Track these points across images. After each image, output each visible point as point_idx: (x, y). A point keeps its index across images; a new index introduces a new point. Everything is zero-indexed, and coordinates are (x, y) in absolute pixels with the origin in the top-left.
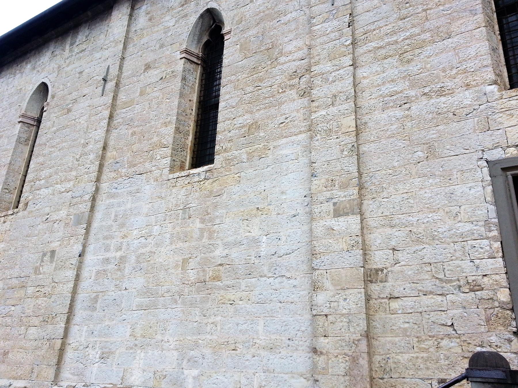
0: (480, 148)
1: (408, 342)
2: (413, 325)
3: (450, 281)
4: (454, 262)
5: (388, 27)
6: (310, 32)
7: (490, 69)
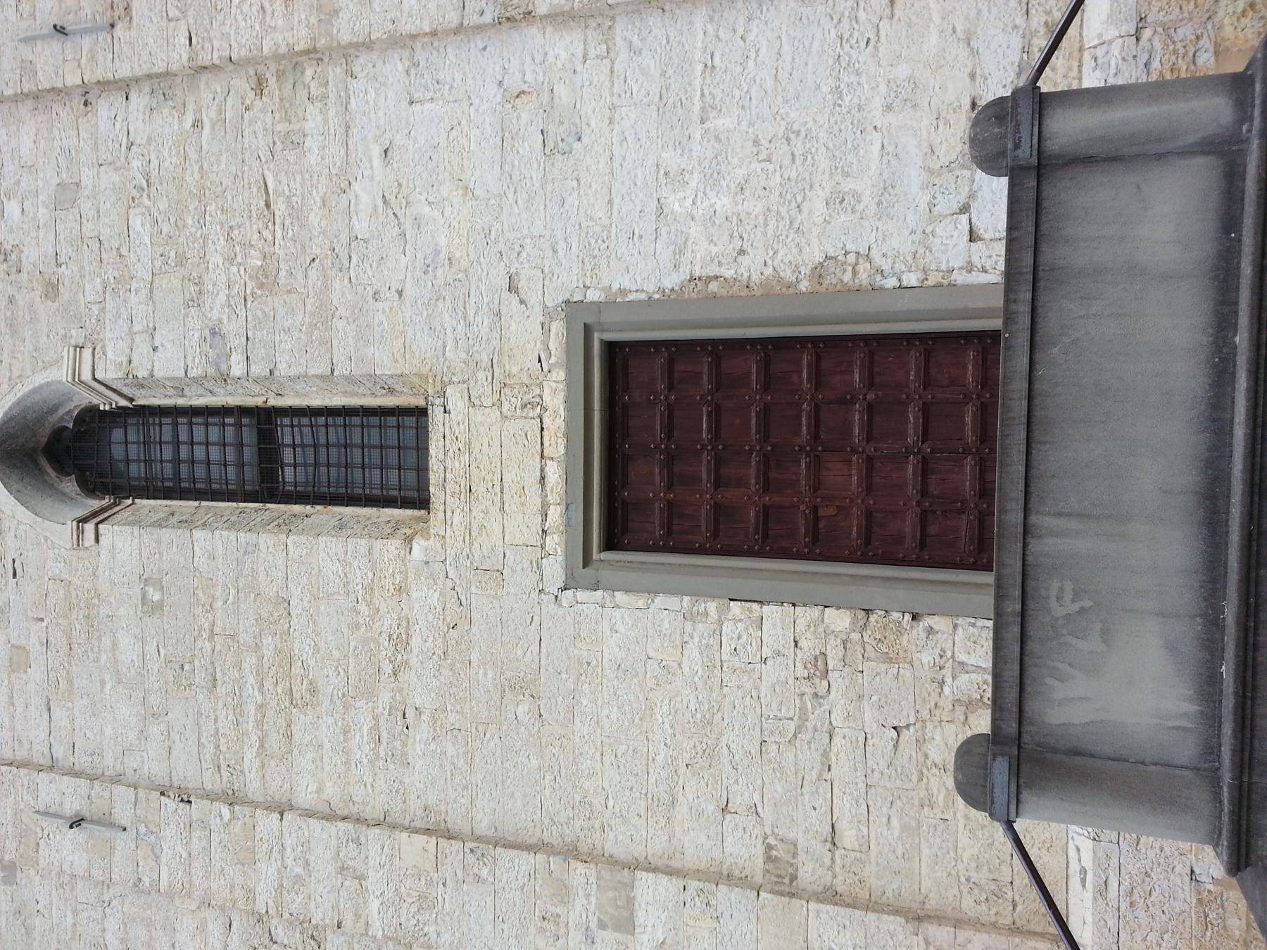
0: (535, 595)
1: (932, 829)
2: (894, 809)
3: (803, 710)
4: (762, 695)
5: (222, 718)
6: (171, 895)
7: (379, 544)
